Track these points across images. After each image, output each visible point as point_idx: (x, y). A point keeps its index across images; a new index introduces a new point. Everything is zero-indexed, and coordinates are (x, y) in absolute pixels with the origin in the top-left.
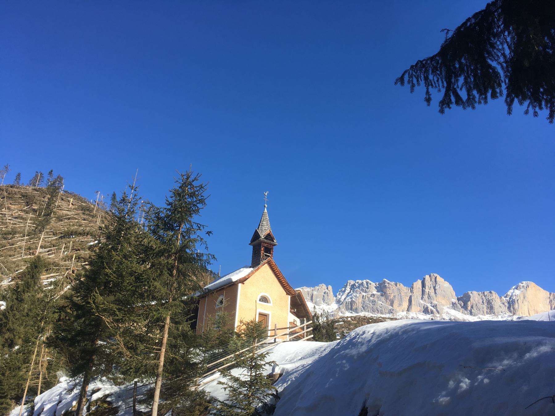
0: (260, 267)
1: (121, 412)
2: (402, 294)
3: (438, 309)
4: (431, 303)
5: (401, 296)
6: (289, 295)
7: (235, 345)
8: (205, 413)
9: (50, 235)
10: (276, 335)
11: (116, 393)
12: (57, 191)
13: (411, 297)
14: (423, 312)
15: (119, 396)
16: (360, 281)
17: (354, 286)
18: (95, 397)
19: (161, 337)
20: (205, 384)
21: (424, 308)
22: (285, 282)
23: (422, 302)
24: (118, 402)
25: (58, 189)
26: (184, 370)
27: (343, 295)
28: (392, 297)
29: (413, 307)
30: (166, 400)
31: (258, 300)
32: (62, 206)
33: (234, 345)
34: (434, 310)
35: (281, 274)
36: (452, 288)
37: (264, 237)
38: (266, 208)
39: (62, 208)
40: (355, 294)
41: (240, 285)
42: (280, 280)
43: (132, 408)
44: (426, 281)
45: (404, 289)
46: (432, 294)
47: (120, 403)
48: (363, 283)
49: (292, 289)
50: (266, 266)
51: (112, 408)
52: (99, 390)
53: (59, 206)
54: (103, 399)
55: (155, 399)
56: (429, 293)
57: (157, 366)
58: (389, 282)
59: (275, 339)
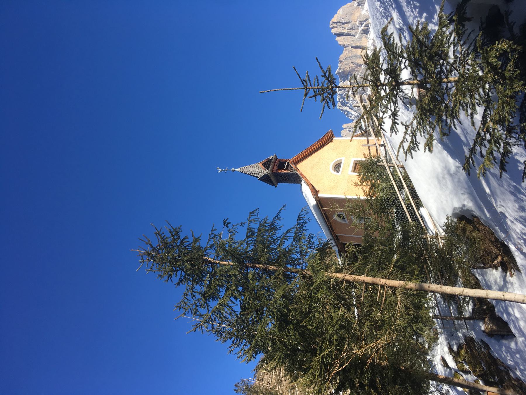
0: (300, 173)
1: (472, 334)
2: (350, 55)
3: (364, 19)
4: (359, 27)
5: (352, 57)
6: (332, 139)
7: (385, 190)
8: (476, 223)
9: (294, 392)
10: (375, 144)
11: (447, 339)
12: (250, 387)
13: (353, 47)
14: (367, 34)
15: (451, 336)
16: (338, 97)
17: (343, 103)
18: (452, 364)
19: (364, 285)
20: (436, 226)
21: (363, 34)
22: (317, 143)
23: (357, 36)
24: (459, 337)
25: (248, 386)
26: (416, 253)
27: (351, 113)
28: (353, 65)
29: (363, 44)
30: (457, 276)
31: (338, 173)
32: (268, 380)
33: (385, 192)
34: (365, 23)
35: (308, 149)
36: (344, 6)
37: (266, 170)
38: (235, 170)
39: (270, 380)
40: (351, 102)
41: (320, 195)
42: (315, 150)
43: (467, 321)
44: (337, 32)
45: (345, 53)
46: (349, 26)
47: (460, 335)
48: (339, 94)
49: (325, 136)
50: (298, 166)
51: (466, 345)
52: (443, 359)
53: (268, 382)
54: (456, 355)
55: (458, 293)
56: (349, 29)
57: (406, 292)
58: (338, 69)
59: (380, 145)
